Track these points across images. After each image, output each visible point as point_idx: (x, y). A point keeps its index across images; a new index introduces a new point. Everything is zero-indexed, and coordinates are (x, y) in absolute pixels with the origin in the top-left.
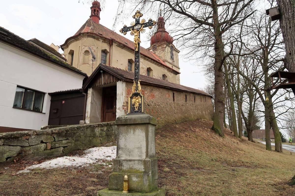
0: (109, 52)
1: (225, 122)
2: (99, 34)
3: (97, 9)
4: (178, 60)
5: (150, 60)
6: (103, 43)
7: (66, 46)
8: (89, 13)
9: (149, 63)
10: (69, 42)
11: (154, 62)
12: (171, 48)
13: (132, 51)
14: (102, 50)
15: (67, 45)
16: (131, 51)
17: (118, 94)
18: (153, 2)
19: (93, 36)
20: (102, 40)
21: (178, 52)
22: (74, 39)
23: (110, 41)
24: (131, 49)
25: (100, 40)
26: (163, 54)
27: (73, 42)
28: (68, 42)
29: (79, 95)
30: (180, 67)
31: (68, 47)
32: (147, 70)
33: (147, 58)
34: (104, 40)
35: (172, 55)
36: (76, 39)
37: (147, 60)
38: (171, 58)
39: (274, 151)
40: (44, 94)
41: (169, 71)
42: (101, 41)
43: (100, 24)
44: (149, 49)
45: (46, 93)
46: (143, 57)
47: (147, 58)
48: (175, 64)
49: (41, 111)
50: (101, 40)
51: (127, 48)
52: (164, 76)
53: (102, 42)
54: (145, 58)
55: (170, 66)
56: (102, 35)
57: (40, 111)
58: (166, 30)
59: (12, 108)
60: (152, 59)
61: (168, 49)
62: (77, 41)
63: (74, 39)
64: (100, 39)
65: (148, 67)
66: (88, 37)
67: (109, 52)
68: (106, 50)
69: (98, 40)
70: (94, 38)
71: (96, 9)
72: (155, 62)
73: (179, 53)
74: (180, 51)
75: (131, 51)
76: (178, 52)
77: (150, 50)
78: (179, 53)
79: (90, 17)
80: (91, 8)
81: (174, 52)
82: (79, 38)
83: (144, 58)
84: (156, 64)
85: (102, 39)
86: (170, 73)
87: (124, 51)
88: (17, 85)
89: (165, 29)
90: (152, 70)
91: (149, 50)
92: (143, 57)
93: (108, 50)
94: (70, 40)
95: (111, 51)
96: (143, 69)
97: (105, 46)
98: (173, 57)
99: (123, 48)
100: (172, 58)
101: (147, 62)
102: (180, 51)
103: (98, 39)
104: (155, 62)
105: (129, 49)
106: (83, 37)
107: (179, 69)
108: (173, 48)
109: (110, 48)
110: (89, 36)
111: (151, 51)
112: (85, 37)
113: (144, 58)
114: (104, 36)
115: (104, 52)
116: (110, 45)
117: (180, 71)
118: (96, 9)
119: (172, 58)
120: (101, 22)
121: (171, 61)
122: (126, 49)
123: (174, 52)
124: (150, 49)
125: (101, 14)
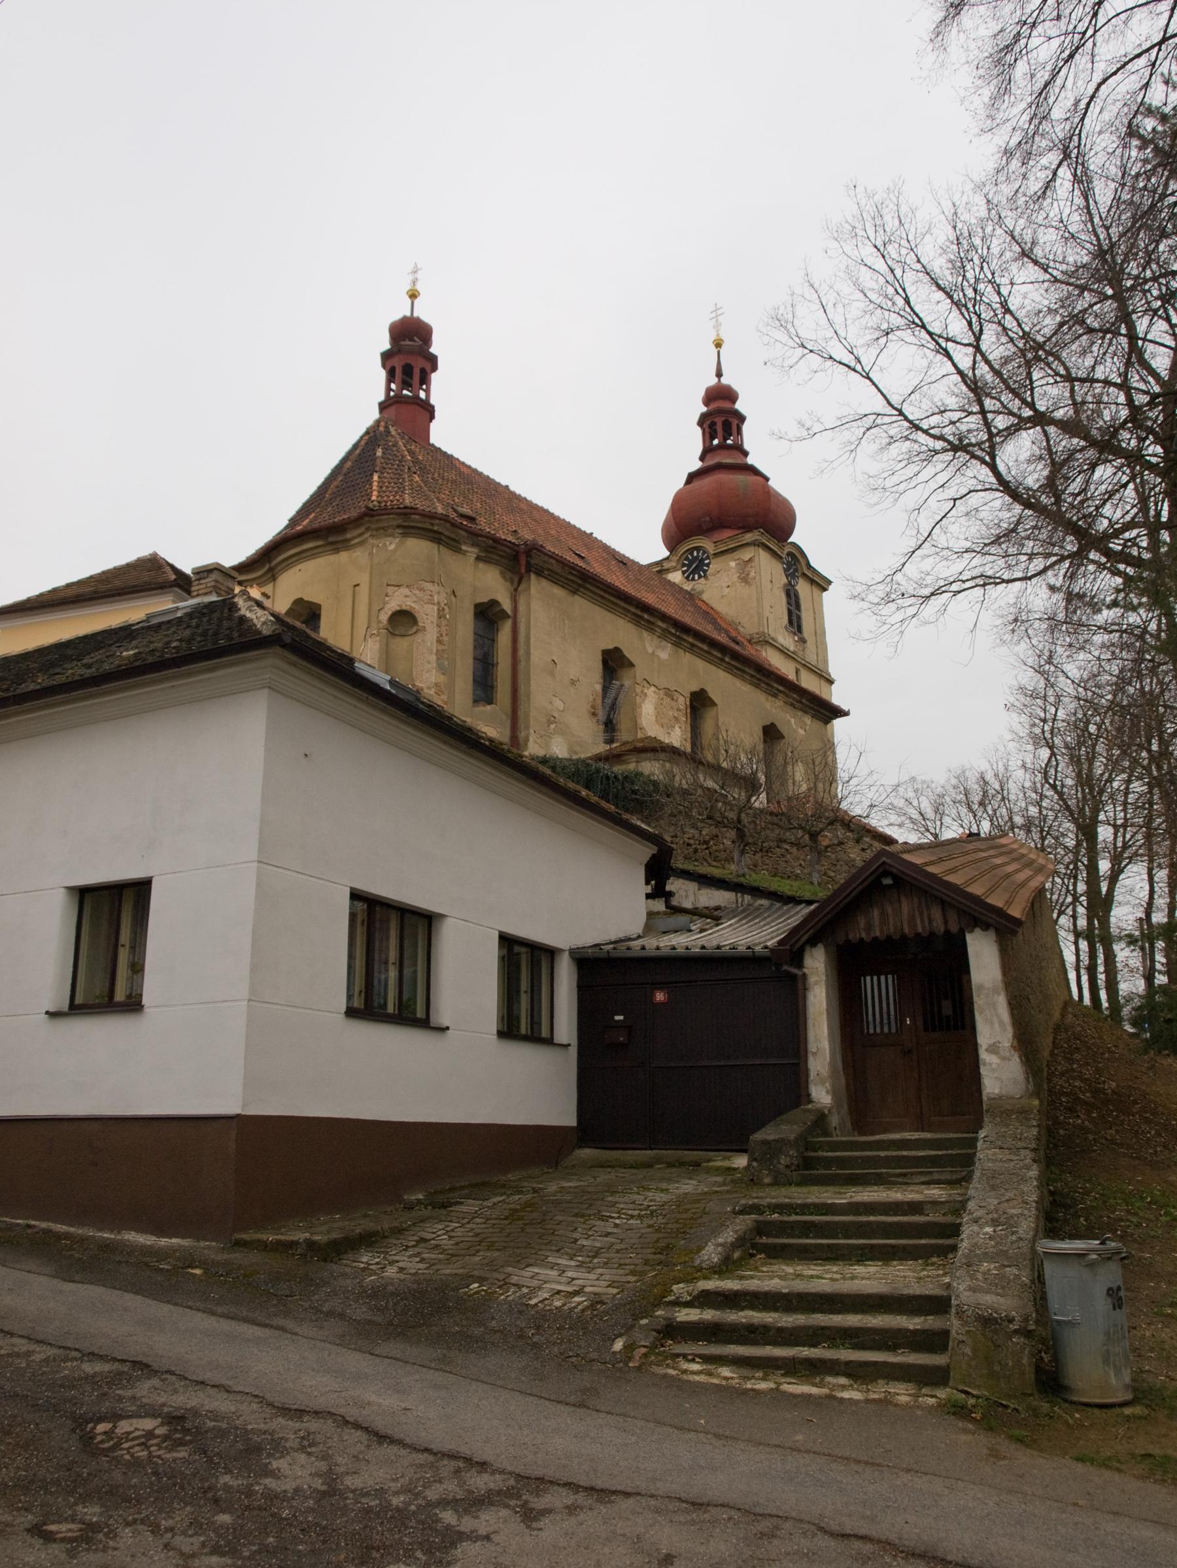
0: (509, 612)
1: (842, 885)
2: (462, 516)
3: (418, 364)
5: (705, 647)
6: (481, 565)
9: (700, 664)
10: (280, 558)
11: (722, 660)
12: (788, 564)
13: (623, 604)
14: (477, 606)
15: (271, 570)
16: (613, 603)
17: (981, 987)
20: (476, 550)
21: (821, 584)
23: (517, 552)
25: (464, 548)
26: (737, 590)
27: (314, 556)
29: (778, 970)
30: (833, 671)
32: (605, 662)
33: (691, 640)
34: (486, 551)
37: (692, 649)
38: (790, 622)
40: (551, 953)
41: (792, 705)
42: (472, 552)
43: (433, 445)
44: (660, 568)
45: (561, 950)
46: (673, 635)
47: (691, 640)
48: (811, 658)
49: (420, 1014)
51: (607, 596)
53: (478, 559)
54: (642, 618)
55: (787, 669)
56: (472, 519)
57: (414, 1012)
58: (750, 460)
59: (342, 1016)
60: (713, 644)
61: (769, 570)
62: (337, 551)
63: (320, 543)
64: (466, 543)
66: (405, 535)
67: (509, 616)
68: (494, 603)
69: (458, 550)
70: (437, 538)
73: (825, 590)
74: (830, 582)
75: (613, 603)
77: (668, 571)
79: (383, 407)
80: (386, 357)
81: (803, 588)
82: (354, 538)
83: (678, 637)
84: (730, 669)
85: (473, 545)
86: (800, 713)
87: (581, 606)
90: (632, 665)
92: (673, 635)
93: (507, 605)
94: (295, 546)
95: (522, 608)
96: (674, 703)
97: (491, 583)
99: (574, 592)
100: (794, 623)
102: (830, 582)
104: (727, 659)
105: (605, 591)
106: (383, 531)
107: (831, 682)
108: (796, 565)
109: (516, 590)
110: (408, 531)
111: (676, 577)
112: (392, 535)
113: (678, 637)
114: (483, 524)
115: (488, 615)
116: (516, 579)
119: (794, 623)
120: (441, 435)
121: (787, 640)
123: (803, 588)
124: (666, 565)
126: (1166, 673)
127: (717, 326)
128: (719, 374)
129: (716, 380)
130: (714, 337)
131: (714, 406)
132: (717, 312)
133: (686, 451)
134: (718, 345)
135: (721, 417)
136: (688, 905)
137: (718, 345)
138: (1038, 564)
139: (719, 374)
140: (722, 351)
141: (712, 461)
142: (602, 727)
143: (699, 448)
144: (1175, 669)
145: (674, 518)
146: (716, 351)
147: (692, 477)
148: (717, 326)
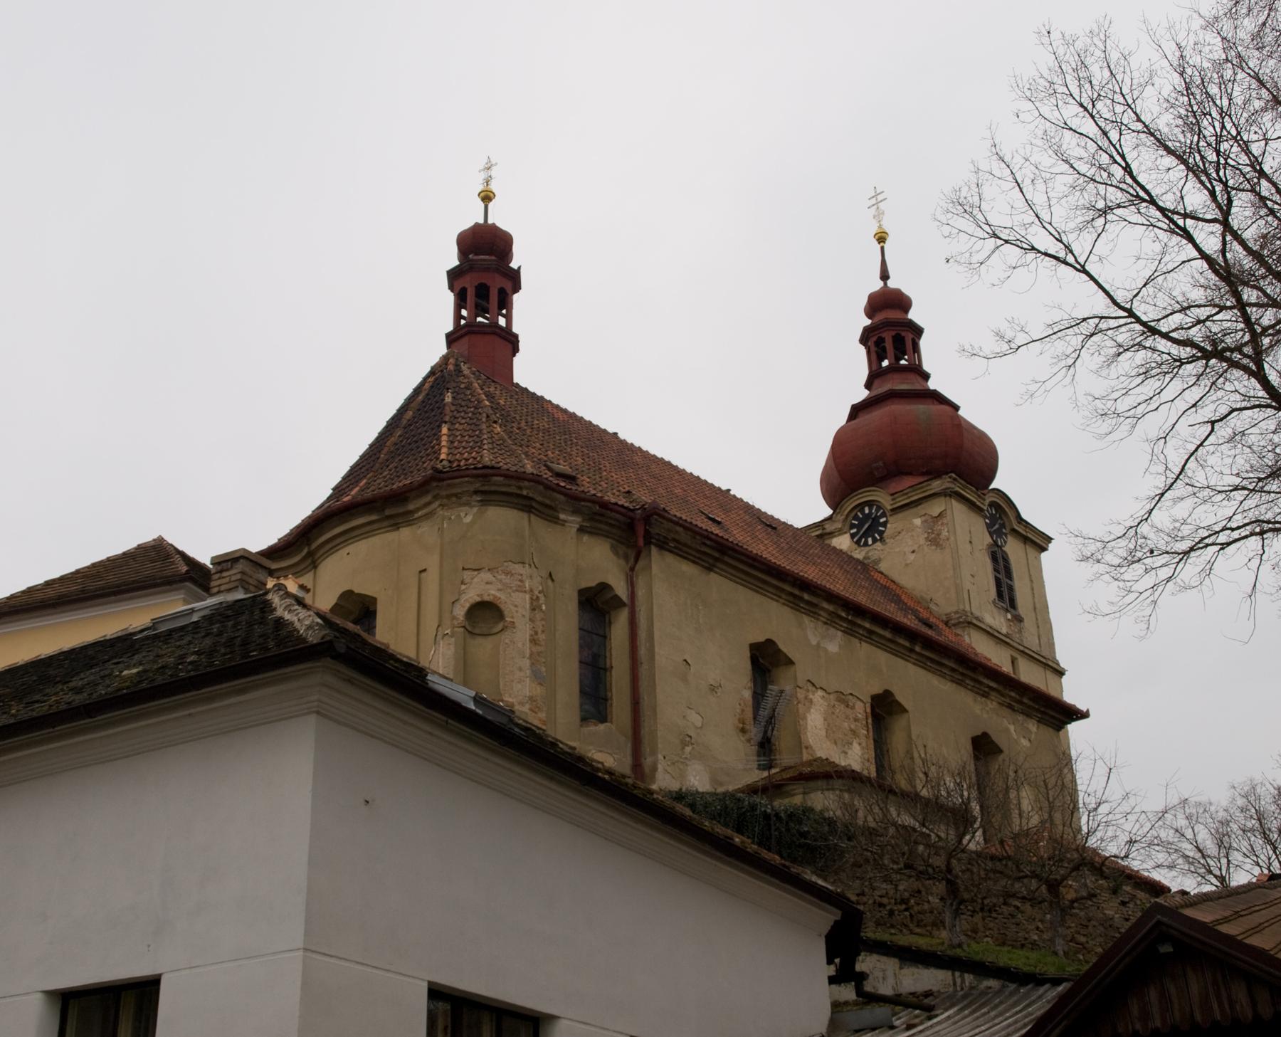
2: (559, 475)
3: (496, 282)
4: (1041, 609)
5: (888, 634)
6: (585, 538)
7: (304, 559)
8: (439, 312)
9: (882, 658)
11: (912, 650)
12: (992, 517)
15: (310, 554)
18: (1213, 423)
19: (525, 493)
20: (579, 519)
21: (1038, 541)
22: (374, 517)
24: (762, 571)
25: (562, 516)
26: (924, 555)
27: (366, 535)
28: (317, 538)
31: (315, 567)
32: (755, 661)
33: (867, 625)
35: (1005, 580)
36: (388, 512)
37: (870, 637)
39: (856, 1003)
41: (1010, 707)
42: (574, 521)
44: (820, 531)
47: (867, 625)
48: (1031, 641)
50: (571, 518)
52: (984, 746)
53: (581, 530)
54: (854, 624)
55: (999, 658)
56: (571, 479)
58: (932, 384)
61: (966, 529)
62: (396, 527)
63: (374, 517)
64: (564, 510)
65: (877, 689)
66: (484, 503)
67: (624, 604)
68: (604, 587)
69: (555, 520)
70: (526, 505)
71: (485, 270)
72: (1025, 700)
73: (1044, 549)
76: (1038, 541)
77: (831, 534)
78: (1044, 555)
79: (451, 339)
80: (453, 275)
81: (1012, 548)
82: (418, 509)
84: (922, 662)
85: (575, 512)
86: (1021, 717)
87: (719, 586)
88: (430, 983)
89: (926, 377)
90: (905, 711)
91: (820, 536)
93: (621, 590)
95: (641, 593)
96: (849, 711)
97: (599, 561)
98: (1011, 589)
99: (709, 569)
100: (1005, 595)
101: (864, 650)
102: (1049, 539)
103: (547, 513)
104: (918, 649)
105: (751, 566)
106: (455, 499)
108: (1003, 518)
109: (632, 569)
110: (488, 497)
111: (843, 542)
112: (467, 504)
114: (587, 485)
117: (1071, 693)
118: (485, 270)
119: (1005, 595)
121: (996, 620)
122: (735, 568)
123: (1012, 548)
124: (829, 527)
125: (525, 314)
127: (879, 216)
128: (885, 276)
129: (881, 284)
130: (875, 230)
131: (880, 317)
132: (877, 199)
134: (881, 239)
135: (891, 330)
137: (881, 239)
139: (885, 276)
141: (882, 388)
148: (879, 216)
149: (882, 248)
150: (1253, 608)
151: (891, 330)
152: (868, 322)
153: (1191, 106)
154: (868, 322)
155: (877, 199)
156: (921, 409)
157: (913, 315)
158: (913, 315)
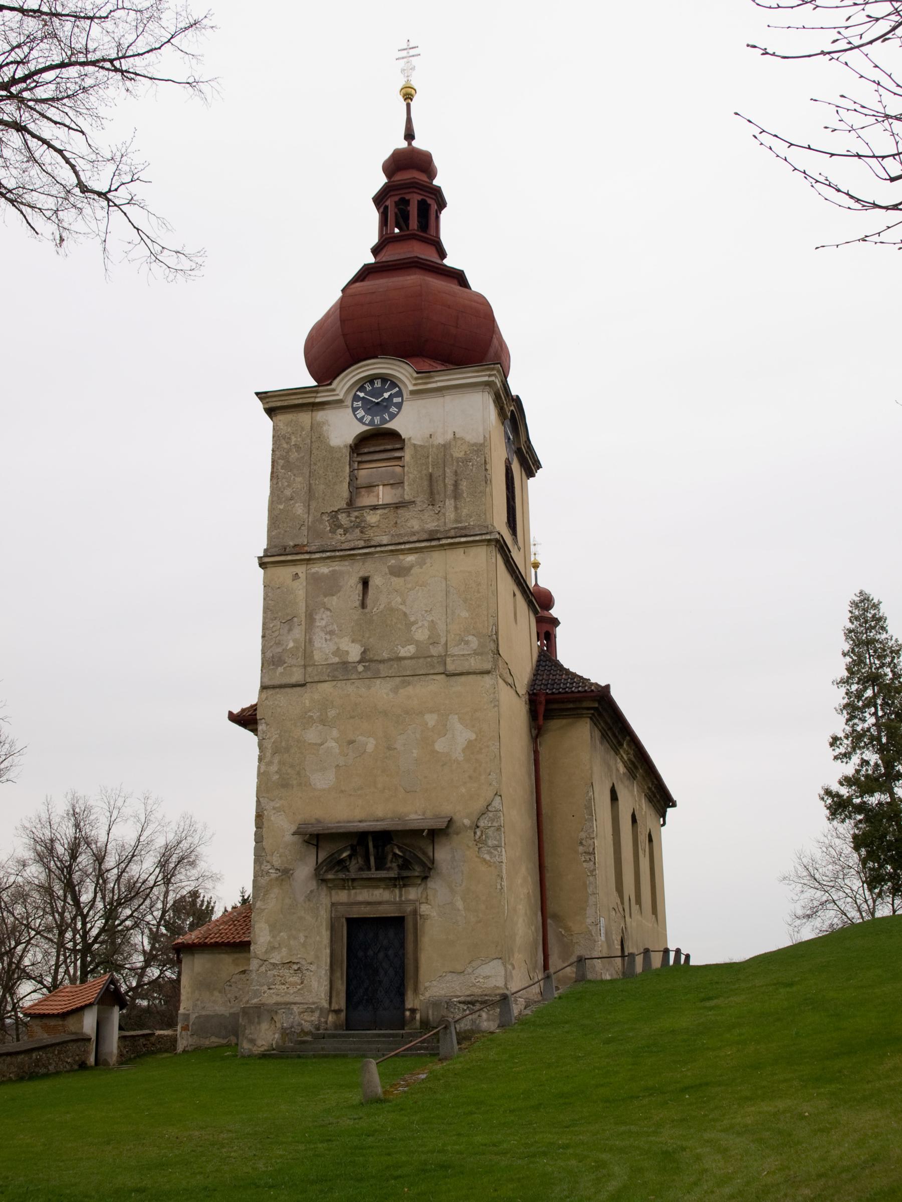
126: (9, 1017)
127: (407, 71)
128: (409, 136)
129: (404, 144)
130: (402, 83)
131: (400, 177)
132: (409, 51)
133: (358, 236)
134: (408, 97)
135: (410, 195)
136: (385, 655)
137: (408, 97)
138: (865, 181)
139: (409, 136)
140: (412, 104)
141: (391, 254)
142: (431, 884)
143: (374, 238)
144: (3, 1019)
145: (343, 321)
146: (405, 104)
147: (366, 273)
148: (407, 71)
149: (408, 106)
150: (874, 82)
151: (410, 195)
152: (371, 259)
153: (24, 188)
154: (371, 259)
155: (409, 51)
156: (456, 288)
157: (554, 612)
158: (554, 612)
